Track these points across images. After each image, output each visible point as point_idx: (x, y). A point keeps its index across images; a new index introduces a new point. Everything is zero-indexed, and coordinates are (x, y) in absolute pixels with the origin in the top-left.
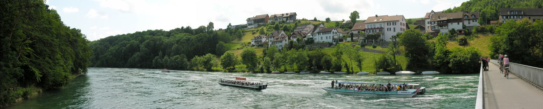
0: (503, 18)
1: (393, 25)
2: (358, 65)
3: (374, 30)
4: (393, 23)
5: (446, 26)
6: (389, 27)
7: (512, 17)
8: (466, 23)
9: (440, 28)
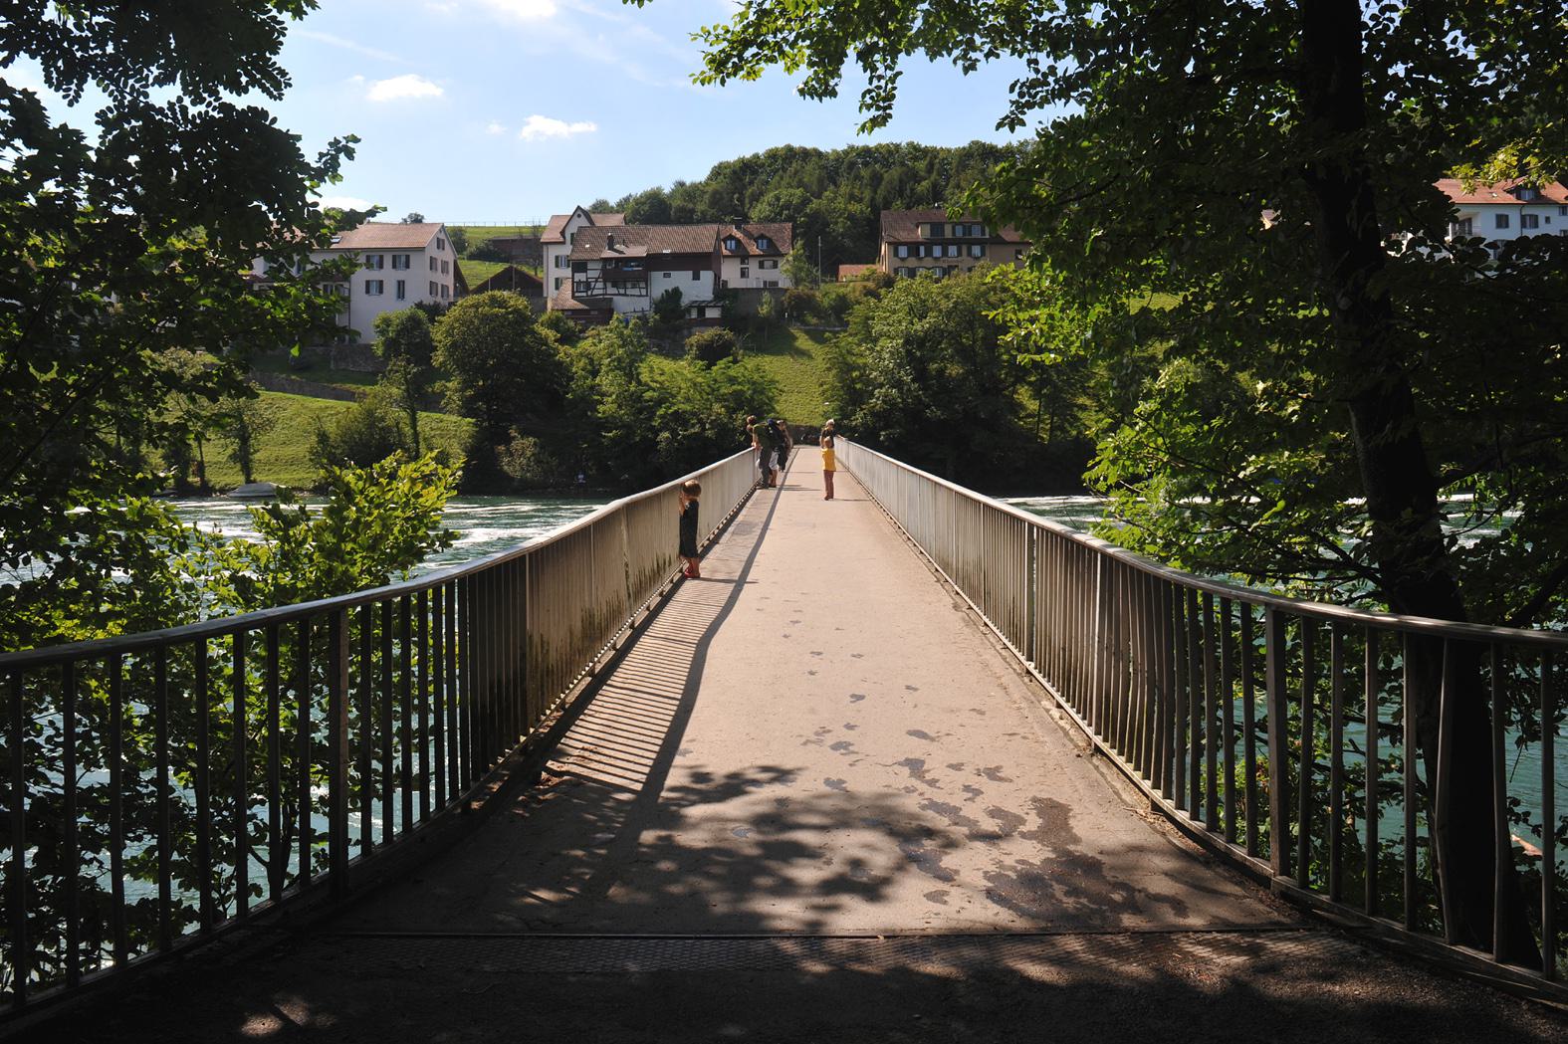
0: (896, 254)
1: (394, 267)
2: (234, 457)
4: (394, 257)
5: (643, 285)
6: (375, 275)
7: (937, 251)
8: (730, 273)
9: (615, 291)
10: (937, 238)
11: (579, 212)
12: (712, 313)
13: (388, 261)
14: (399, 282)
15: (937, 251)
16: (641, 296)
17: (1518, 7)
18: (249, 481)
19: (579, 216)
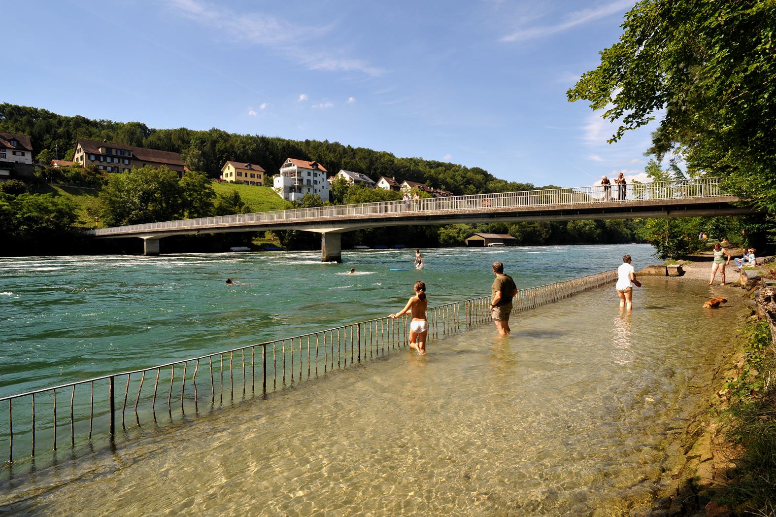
7: (109, 160)
10: (109, 153)
15: (109, 160)
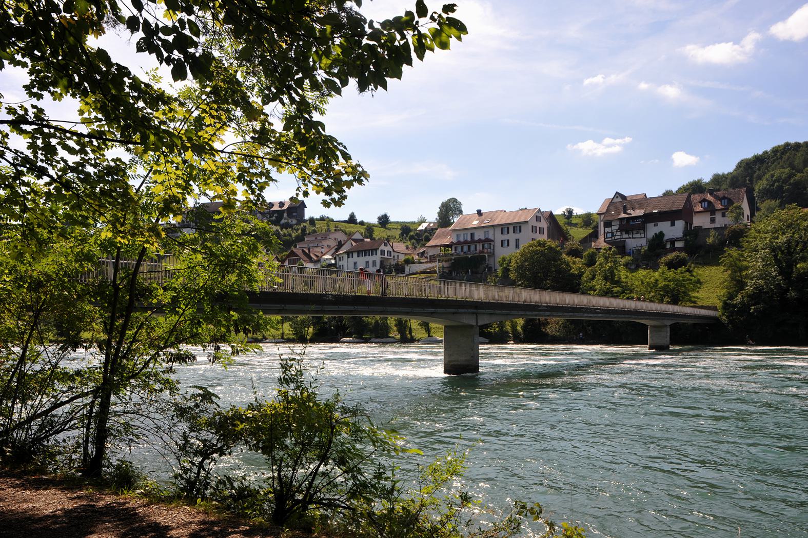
1: (514, 232)
3: (473, 248)
4: (514, 228)
5: (642, 231)
6: (505, 237)
9: (627, 236)
11: (617, 195)
12: (679, 245)
13: (511, 230)
14: (516, 240)
16: (641, 238)
17: (251, 28)
18: (429, 336)
19: (617, 197)
